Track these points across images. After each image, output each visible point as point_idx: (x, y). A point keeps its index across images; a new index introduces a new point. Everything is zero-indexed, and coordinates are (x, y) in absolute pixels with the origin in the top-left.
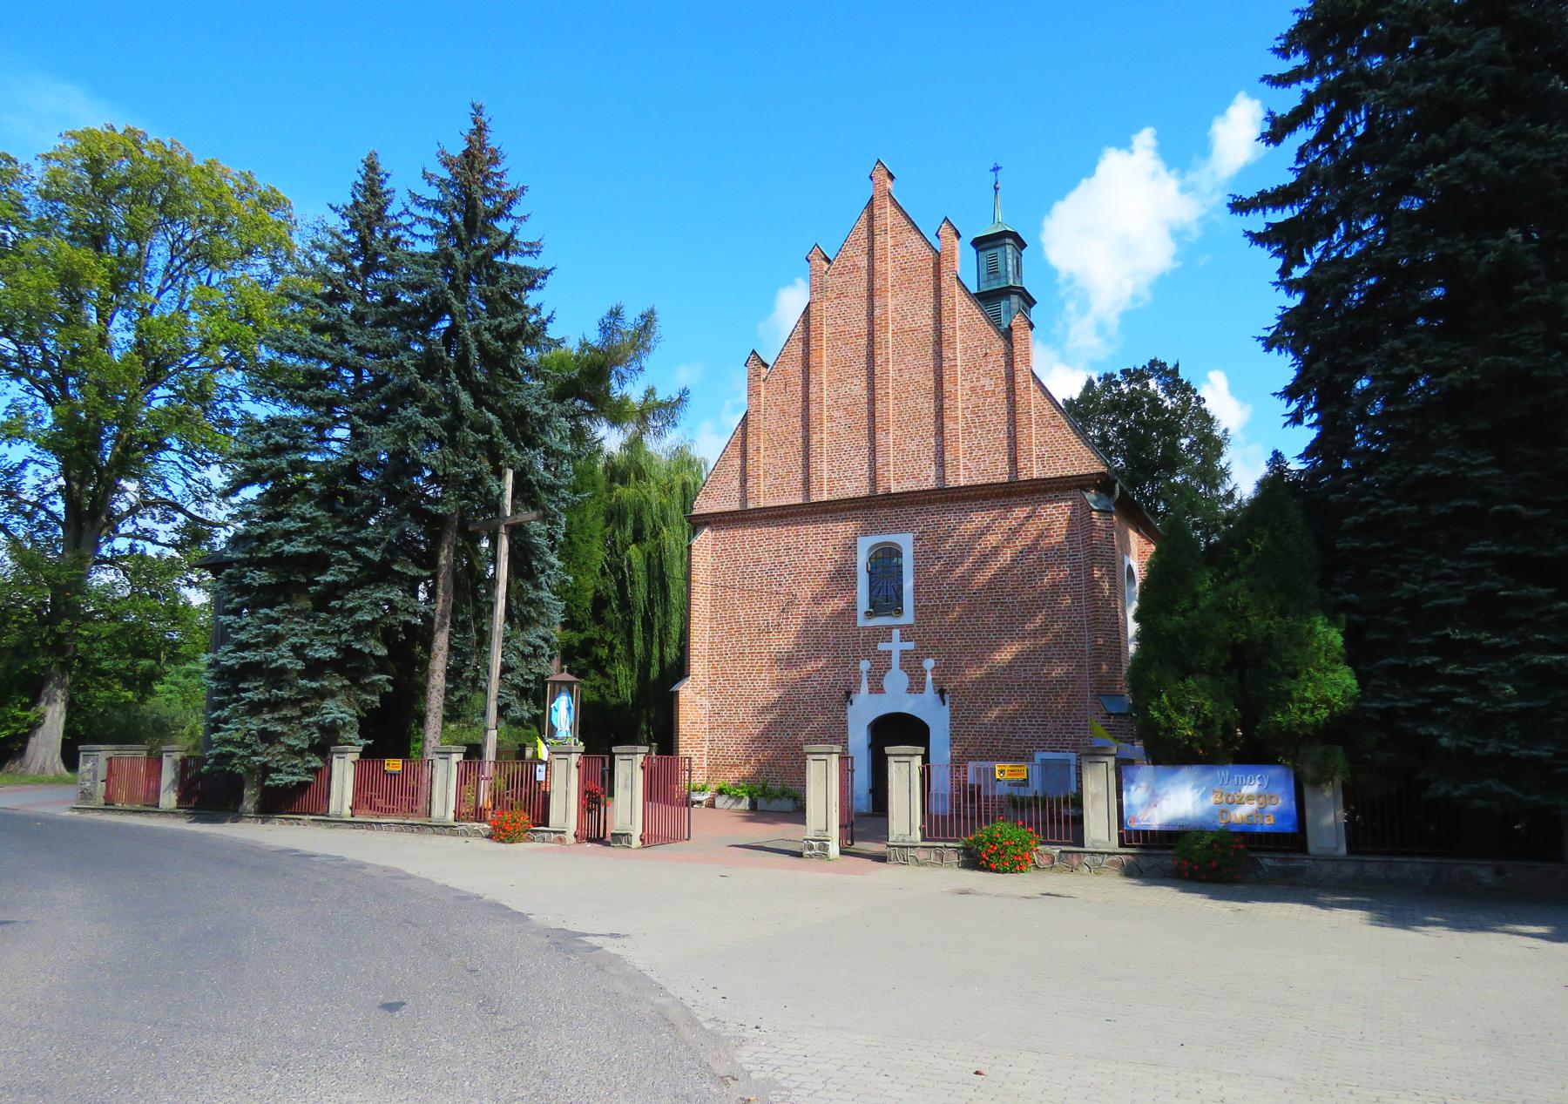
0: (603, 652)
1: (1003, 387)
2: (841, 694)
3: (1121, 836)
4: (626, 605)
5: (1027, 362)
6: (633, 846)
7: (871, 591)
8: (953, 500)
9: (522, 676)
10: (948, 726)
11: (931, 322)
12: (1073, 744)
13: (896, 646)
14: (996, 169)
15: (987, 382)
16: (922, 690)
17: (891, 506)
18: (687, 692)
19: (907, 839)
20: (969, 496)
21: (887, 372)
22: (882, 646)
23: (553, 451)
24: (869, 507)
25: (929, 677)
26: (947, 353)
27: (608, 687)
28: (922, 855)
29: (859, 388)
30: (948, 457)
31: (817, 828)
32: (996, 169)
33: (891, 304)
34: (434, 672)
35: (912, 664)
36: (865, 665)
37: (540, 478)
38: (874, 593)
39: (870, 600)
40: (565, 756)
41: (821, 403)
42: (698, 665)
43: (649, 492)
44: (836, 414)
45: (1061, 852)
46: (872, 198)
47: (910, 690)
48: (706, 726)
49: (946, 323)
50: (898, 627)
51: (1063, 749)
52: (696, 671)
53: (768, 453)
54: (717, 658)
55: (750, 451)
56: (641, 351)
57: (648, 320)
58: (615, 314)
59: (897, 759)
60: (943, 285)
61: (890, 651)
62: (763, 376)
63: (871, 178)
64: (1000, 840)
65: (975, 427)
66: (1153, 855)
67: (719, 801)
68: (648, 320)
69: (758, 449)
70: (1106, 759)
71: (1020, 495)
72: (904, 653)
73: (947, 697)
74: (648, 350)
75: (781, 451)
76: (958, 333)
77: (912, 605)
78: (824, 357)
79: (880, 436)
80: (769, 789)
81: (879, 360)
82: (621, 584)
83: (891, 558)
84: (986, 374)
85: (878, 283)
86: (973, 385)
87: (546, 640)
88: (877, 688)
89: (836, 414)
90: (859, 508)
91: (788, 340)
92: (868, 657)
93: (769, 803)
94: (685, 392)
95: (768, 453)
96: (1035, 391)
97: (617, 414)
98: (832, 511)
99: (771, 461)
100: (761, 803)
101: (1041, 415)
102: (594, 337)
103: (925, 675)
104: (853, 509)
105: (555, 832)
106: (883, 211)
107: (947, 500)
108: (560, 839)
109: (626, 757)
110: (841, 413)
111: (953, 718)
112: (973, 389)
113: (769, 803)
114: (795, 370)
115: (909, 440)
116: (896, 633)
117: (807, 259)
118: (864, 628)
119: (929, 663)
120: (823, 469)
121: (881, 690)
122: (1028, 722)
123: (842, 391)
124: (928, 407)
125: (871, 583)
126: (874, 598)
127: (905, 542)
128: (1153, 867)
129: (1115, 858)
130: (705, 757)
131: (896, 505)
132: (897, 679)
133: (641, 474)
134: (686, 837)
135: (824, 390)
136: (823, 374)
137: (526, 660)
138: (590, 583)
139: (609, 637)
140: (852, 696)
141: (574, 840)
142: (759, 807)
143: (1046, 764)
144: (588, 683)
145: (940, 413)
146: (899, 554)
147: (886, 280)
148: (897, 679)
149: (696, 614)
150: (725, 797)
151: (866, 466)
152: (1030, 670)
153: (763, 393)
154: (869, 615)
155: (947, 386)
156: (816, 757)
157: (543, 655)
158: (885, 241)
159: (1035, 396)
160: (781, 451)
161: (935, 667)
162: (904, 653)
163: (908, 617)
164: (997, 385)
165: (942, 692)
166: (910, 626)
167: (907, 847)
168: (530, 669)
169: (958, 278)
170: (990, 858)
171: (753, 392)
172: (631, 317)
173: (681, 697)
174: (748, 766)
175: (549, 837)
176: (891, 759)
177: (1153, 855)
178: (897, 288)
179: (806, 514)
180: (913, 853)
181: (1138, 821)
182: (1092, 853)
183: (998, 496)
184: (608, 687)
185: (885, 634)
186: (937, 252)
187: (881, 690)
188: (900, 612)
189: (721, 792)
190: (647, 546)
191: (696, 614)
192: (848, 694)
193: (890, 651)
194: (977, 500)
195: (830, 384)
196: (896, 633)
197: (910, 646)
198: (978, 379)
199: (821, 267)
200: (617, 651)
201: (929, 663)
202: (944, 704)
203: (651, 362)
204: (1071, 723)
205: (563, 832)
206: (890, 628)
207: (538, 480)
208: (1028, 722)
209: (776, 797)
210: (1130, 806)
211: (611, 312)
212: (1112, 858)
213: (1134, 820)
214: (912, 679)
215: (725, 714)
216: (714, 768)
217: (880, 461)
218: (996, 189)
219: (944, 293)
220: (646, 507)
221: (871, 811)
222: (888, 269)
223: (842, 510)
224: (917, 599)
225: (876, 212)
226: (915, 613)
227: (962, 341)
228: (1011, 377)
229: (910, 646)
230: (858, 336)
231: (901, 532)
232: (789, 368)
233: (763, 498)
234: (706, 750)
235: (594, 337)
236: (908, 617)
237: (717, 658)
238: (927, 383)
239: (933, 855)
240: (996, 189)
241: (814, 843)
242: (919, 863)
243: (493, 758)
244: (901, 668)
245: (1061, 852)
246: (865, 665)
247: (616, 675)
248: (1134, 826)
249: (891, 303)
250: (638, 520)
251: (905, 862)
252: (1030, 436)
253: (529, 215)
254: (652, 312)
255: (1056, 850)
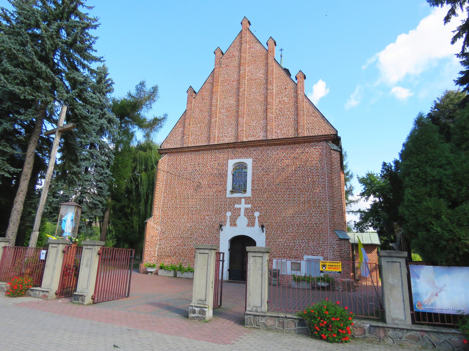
0: (129, 211)
1: (293, 101)
2: (217, 226)
3: (412, 315)
4: (139, 195)
5: (303, 91)
6: (86, 303)
7: (233, 183)
8: (270, 145)
9: (88, 216)
10: (265, 242)
11: (263, 76)
12: (321, 252)
13: (243, 206)
14: (281, 50)
15: (286, 100)
16: (253, 225)
17: (244, 147)
18: (150, 223)
19: (259, 310)
20: (277, 143)
21: (244, 94)
22: (237, 206)
23: (90, 102)
24: (234, 147)
25: (257, 220)
26: (270, 87)
27: (129, 224)
28: (270, 322)
29: (232, 101)
30: (269, 128)
31: (240, 216)
32: (281, 50)
33: (247, 69)
34: (17, 202)
35: (249, 214)
36: (229, 214)
37: (81, 112)
38: (234, 183)
39: (232, 186)
40: (56, 245)
41: (217, 106)
42: (157, 212)
43: (152, 154)
44: (222, 111)
45: (371, 326)
46: (242, 31)
47: (248, 225)
48: (158, 238)
49: (269, 76)
50: (245, 198)
51: (317, 254)
52: (156, 214)
53: (193, 126)
54: (165, 209)
55: (187, 125)
56: (152, 101)
57: (155, 89)
58: (142, 84)
59: (253, 254)
60: (269, 62)
61: (240, 208)
62: (194, 96)
63: (241, 23)
64: (328, 316)
65: (280, 116)
66: (442, 333)
67: (161, 272)
68: (155, 89)
69: (190, 124)
70: (399, 260)
71: (299, 143)
72: (246, 209)
73: (264, 229)
74: (154, 101)
75: (199, 125)
76: (274, 80)
77: (251, 184)
78: (219, 89)
79: (240, 119)
80: (183, 267)
81: (241, 90)
82: (137, 186)
83: (242, 169)
84: (285, 96)
85: (243, 61)
86: (280, 100)
87: (101, 202)
88: (233, 224)
89: (222, 111)
90: (230, 148)
91: (205, 83)
92: (230, 211)
93: (182, 274)
94: (166, 115)
95: (193, 126)
96: (306, 102)
97: (141, 123)
98: (218, 149)
99: (194, 129)
100: (179, 274)
101: (308, 112)
102: (134, 92)
103: (255, 219)
104: (227, 148)
105: (43, 291)
106: (246, 35)
107: (268, 145)
108: (45, 295)
109: (89, 247)
110: (225, 110)
111: (267, 238)
112: (280, 102)
113: (182, 274)
114: (206, 94)
115: (252, 121)
116: (243, 200)
117: (214, 52)
118: (230, 198)
119: (257, 214)
120: (216, 132)
121: (235, 225)
122: (301, 242)
123: (225, 102)
124: (260, 108)
125: (233, 179)
126: (234, 186)
127: (249, 162)
128: (443, 342)
129: (413, 333)
130: (156, 252)
131: (245, 147)
132: (242, 220)
133: (151, 148)
134: (126, 295)
135: (218, 100)
136: (218, 96)
137: (91, 210)
138: (124, 183)
139: (131, 205)
140: (222, 227)
141: (55, 296)
142: (178, 276)
143: (308, 261)
144: (121, 222)
145: (266, 111)
146: (246, 168)
147: (246, 60)
148: (242, 220)
149: (158, 190)
150: (163, 270)
151: (234, 131)
152: (302, 218)
153: (193, 103)
154: (232, 192)
155: (269, 100)
156: (202, 251)
157: (99, 208)
158: (246, 46)
159: (306, 105)
160: (199, 125)
161: (260, 216)
162: (246, 209)
163: (249, 193)
164: (290, 100)
165: (262, 227)
166: (250, 198)
167: (259, 316)
168: (92, 213)
169: (275, 59)
170: (320, 329)
171: (189, 102)
172: (148, 87)
173: (148, 225)
174: (175, 257)
175: (39, 294)
176: (250, 255)
177: (442, 333)
178: (250, 64)
179: (207, 150)
180: (263, 320)
181: (424, 306)
182: (394, 329)
183: (289, 144)
184: (129, 224)
185: (238, 200)
186: (266, 50)
187: (235, 225)
188: (245, 191)
189: (161, 268)
190: (149, 173)
191: (158, 190)
192: (221, 226)
193: (240, 208)
194: (281, 145)
195: (221, 99)
196: (243, 200)
197: (249, 206)
198: (282, 98)
199: (220, 56)
200: (134, 211)
201: (257, 214)
202: (263, 232)
203: (154, 105)
204: (320, 242)
205: (47, 292)
206: (241, 198)
207: (80, 113)
208: (301, 242)
209: (186, 271)
210: (417, 294)
211: (141, 83)
212: (409, 333)
213: (421, 305)
214: (249, 220)
215: (167, 233)
216: (160, 257)
217: (240, 129)
218: (281, 56)
219: (269, 65)
220: (149, 159)
221: (228, 279)
222: (247, 56)
223: (223, 148)
224: (253, 186)
225: (243, 35)
226: (252, 192)
227: (276, 83)
228: (296, 97)
229: (249, 206)
230: (233, 81)
231: (247, 158)
232: (204, 93)
233: (191, 142)
234: (157, 248)
235: (134, 92)
236: (249, 193)
237: (165, 209)
238: (260, 99)
239: (277, 323)
240: (281, 56)
241: (196, 309)
242: (268, 329)
243: (34, 246)
244: (245, 216)
245: (371, 326)
246: (229, 214)
247: (133, 220)
248: (421, 309)
249: (247, 69)
250: (146, 164)
251: (258, 327)
252: (304, 120)
253: (93, 7)
254: (157, 87)
255: (367, 324)
